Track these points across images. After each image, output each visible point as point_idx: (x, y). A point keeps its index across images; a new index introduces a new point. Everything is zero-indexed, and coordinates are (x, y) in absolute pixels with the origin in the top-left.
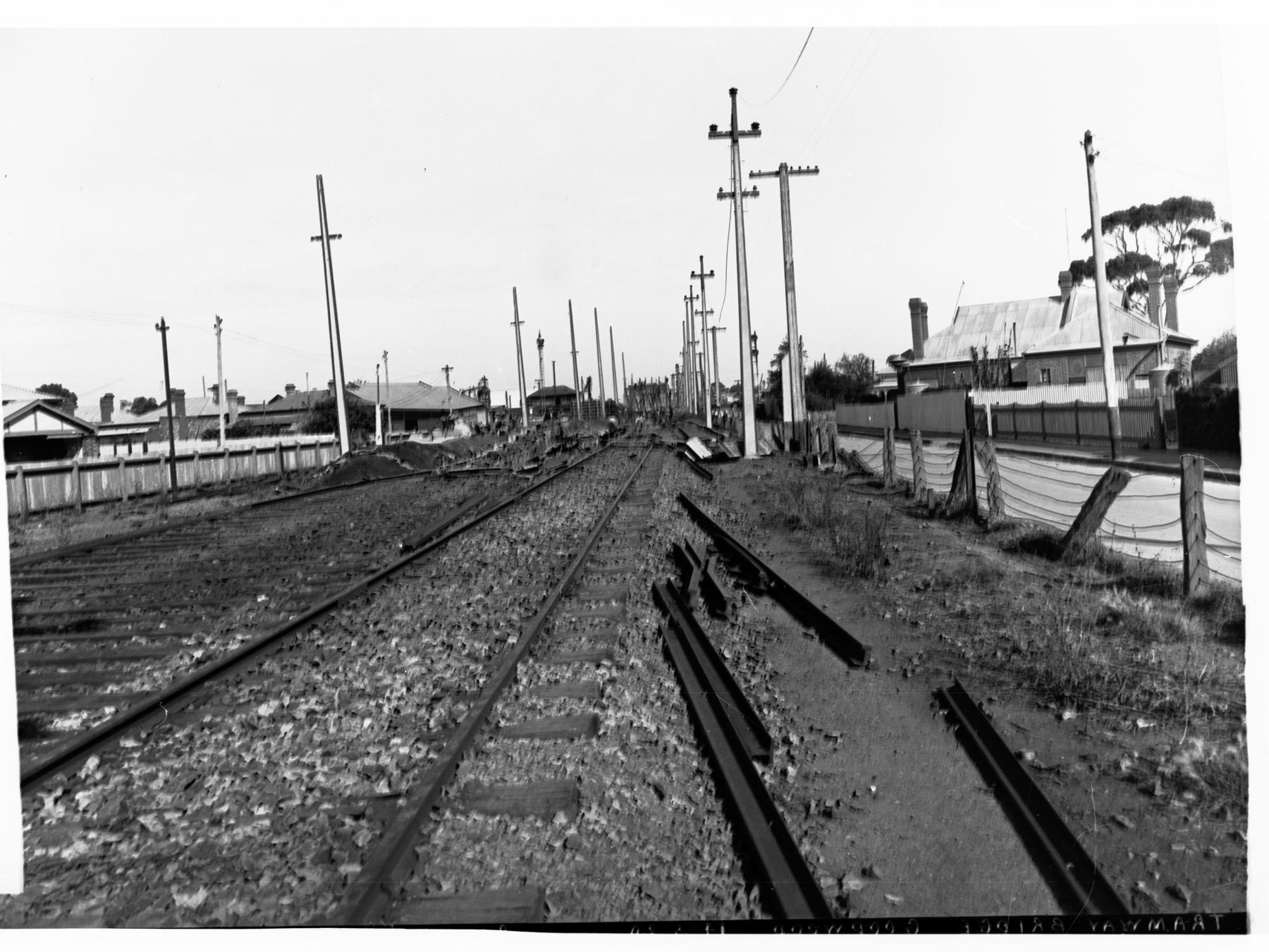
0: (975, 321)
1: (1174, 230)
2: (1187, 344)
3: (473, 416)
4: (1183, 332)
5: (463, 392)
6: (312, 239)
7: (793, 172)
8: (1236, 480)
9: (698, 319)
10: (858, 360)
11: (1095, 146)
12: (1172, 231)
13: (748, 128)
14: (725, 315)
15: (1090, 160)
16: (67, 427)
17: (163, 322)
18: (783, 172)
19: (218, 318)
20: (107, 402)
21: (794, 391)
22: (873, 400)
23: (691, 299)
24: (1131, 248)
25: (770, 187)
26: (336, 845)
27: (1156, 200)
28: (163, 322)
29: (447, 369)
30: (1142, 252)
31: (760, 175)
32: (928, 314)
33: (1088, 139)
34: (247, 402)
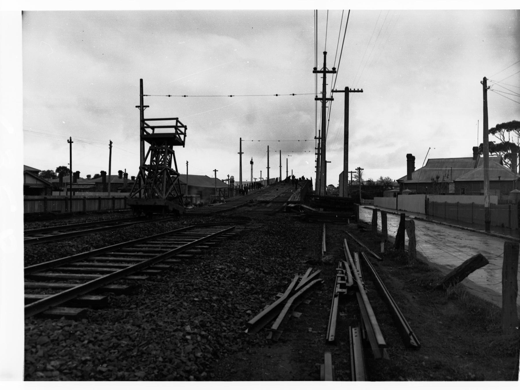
5: (223, 181)
6: (136, 107)
7: (351, 91)
10: (386, 179)
11: (488, 84)
13: (331, 70)
16: (38, 183)
17: (71, 140)
18: (347, 91)
20: (395, 180)
24: (506, 140)
25: (340, 98)
26: (203, 361)
29: (215, 171)
30: (511, 141)
31: (336, 91)
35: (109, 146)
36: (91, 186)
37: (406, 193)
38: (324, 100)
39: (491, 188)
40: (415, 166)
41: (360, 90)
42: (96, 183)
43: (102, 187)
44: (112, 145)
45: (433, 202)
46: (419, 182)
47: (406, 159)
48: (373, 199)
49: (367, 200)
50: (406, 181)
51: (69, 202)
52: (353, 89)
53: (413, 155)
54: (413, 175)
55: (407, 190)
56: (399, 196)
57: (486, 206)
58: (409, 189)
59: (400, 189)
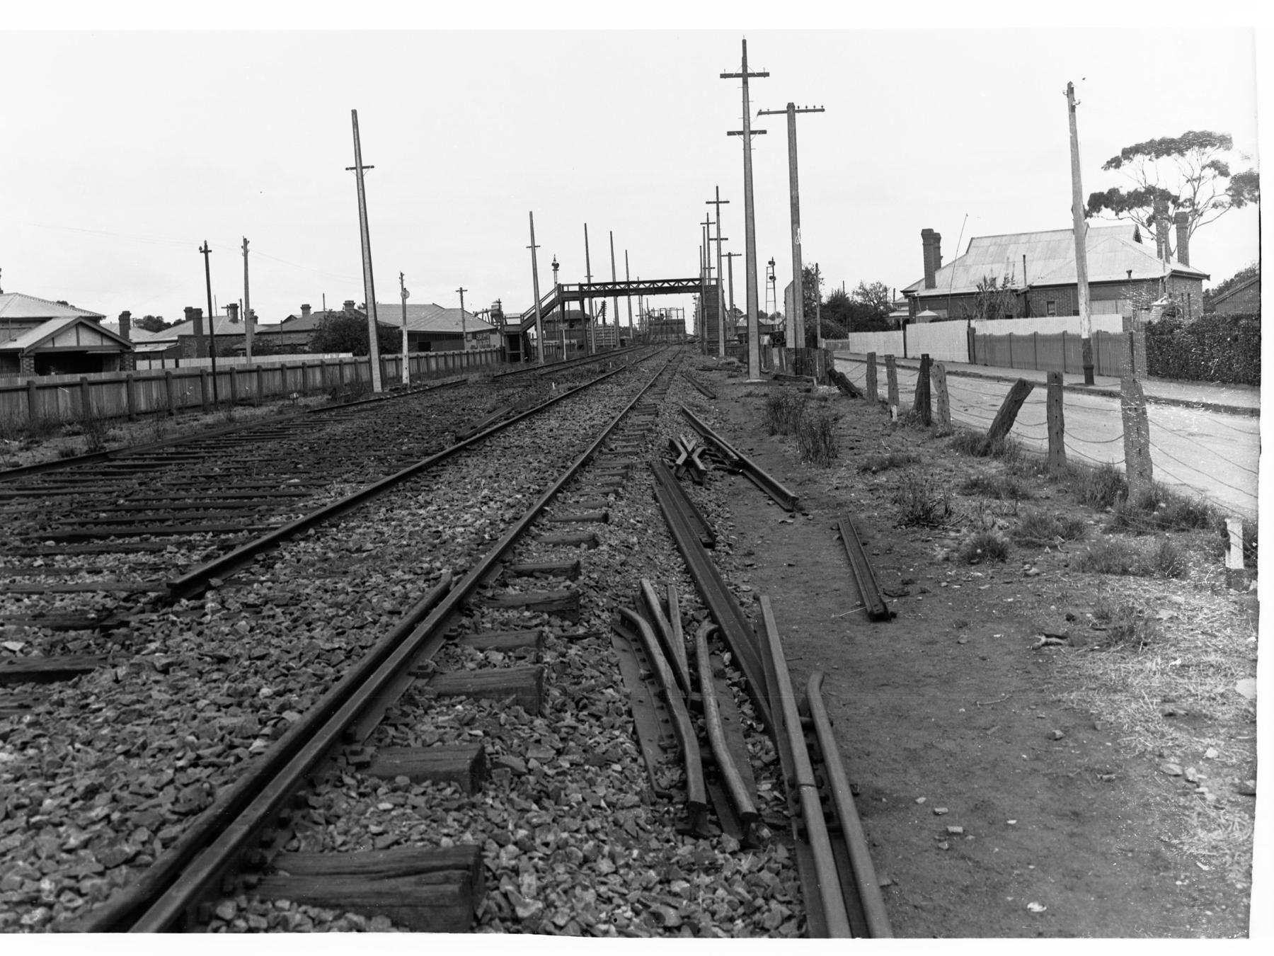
0: (987, 251)
1: (1194, 162)
2: (1198, 278)
3: (486, 338)
4: (1195, 266)
5: (476, 314)
8: (1255, 413)
9: (713, 244)
11: (1077, 95)
12: (1193, 159)
14: (736, 243)
15: (1073, 109)
16: (107, 343)
17: (206, 246)
19: (245, 240)
20: (125, 317)
21: (293, 336)
22: (885, 327)
23: (708, 224)
27: (1176, 135)
28: (206, 246)
29: (461, 291)
32: (942, 244)
33: (1071, 90)
34: (260, 322)
35: (242, 251)
36: (168, 345)
37: (924, 319)
38: (747, 133)
39: (1093, 298)
40: (942, 253)
41: (818, 107)
42: (181, 337)
43: (195, 345)
44: (249, 246)
45: (985, 336)
46: (953, 292)
47: (921, 241)
48: (847, 337)
49: (832, 341)
50: (923, 292)
51: (210, 380)
52: (803, 108)
53: (935, 231)
54: (939, 277)
55: (927, 313)
56: (908, 326)
57: (1085, 336)
58: (930, 309)
59: (910, 311)
